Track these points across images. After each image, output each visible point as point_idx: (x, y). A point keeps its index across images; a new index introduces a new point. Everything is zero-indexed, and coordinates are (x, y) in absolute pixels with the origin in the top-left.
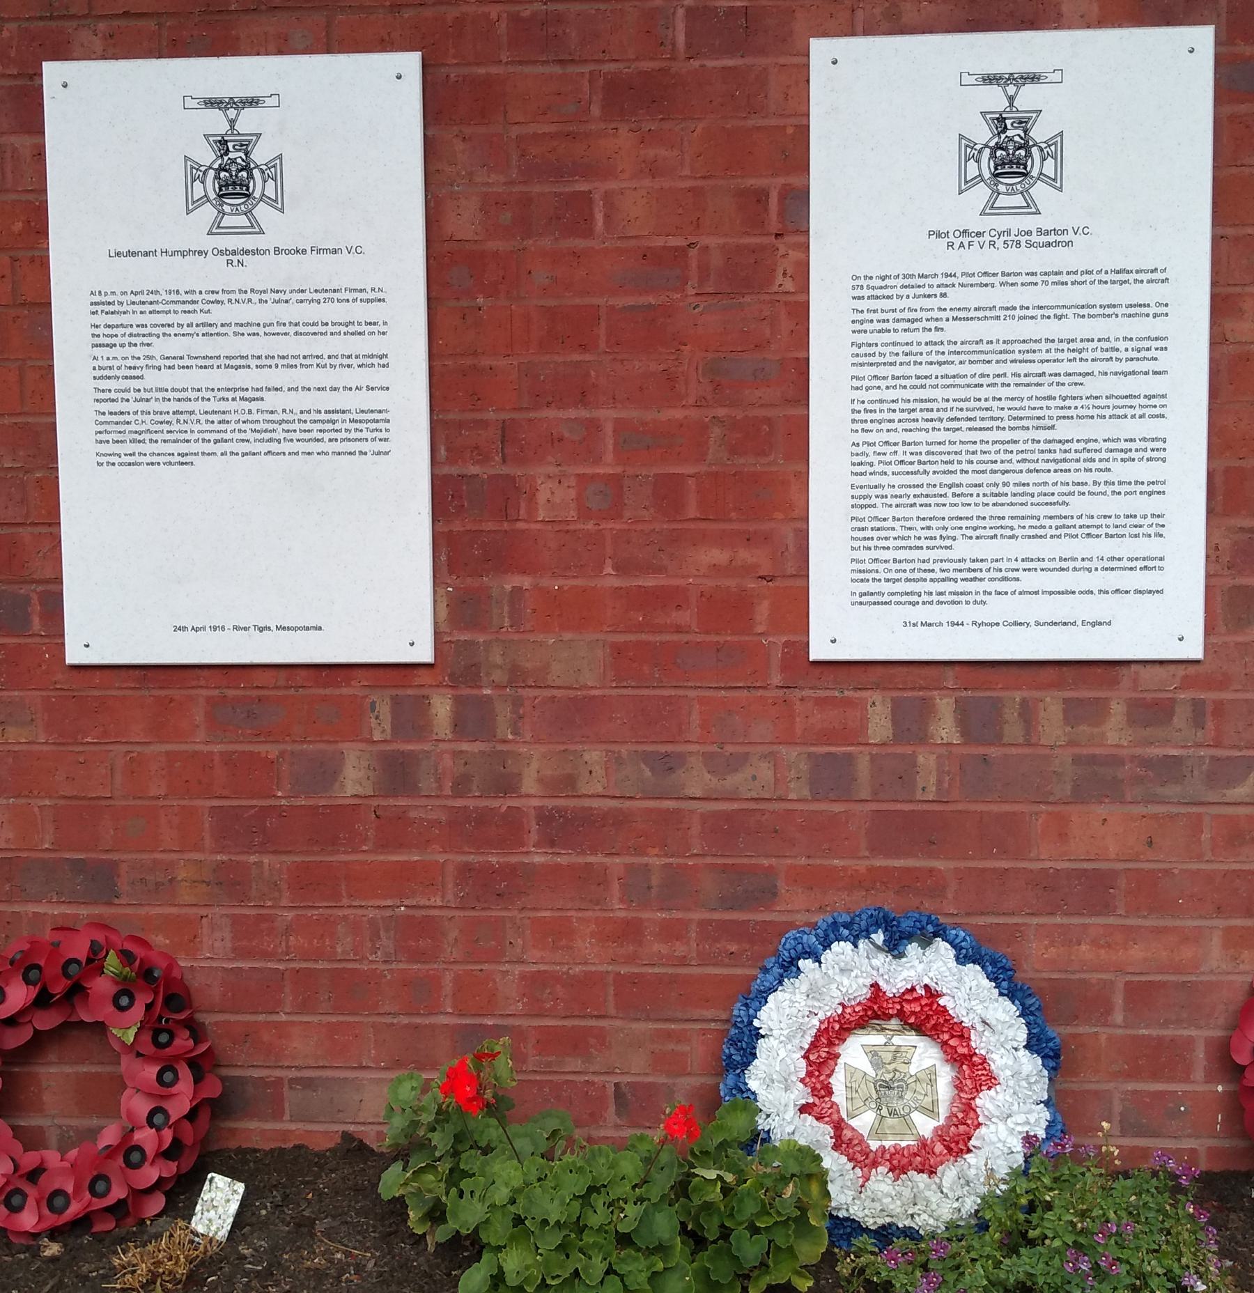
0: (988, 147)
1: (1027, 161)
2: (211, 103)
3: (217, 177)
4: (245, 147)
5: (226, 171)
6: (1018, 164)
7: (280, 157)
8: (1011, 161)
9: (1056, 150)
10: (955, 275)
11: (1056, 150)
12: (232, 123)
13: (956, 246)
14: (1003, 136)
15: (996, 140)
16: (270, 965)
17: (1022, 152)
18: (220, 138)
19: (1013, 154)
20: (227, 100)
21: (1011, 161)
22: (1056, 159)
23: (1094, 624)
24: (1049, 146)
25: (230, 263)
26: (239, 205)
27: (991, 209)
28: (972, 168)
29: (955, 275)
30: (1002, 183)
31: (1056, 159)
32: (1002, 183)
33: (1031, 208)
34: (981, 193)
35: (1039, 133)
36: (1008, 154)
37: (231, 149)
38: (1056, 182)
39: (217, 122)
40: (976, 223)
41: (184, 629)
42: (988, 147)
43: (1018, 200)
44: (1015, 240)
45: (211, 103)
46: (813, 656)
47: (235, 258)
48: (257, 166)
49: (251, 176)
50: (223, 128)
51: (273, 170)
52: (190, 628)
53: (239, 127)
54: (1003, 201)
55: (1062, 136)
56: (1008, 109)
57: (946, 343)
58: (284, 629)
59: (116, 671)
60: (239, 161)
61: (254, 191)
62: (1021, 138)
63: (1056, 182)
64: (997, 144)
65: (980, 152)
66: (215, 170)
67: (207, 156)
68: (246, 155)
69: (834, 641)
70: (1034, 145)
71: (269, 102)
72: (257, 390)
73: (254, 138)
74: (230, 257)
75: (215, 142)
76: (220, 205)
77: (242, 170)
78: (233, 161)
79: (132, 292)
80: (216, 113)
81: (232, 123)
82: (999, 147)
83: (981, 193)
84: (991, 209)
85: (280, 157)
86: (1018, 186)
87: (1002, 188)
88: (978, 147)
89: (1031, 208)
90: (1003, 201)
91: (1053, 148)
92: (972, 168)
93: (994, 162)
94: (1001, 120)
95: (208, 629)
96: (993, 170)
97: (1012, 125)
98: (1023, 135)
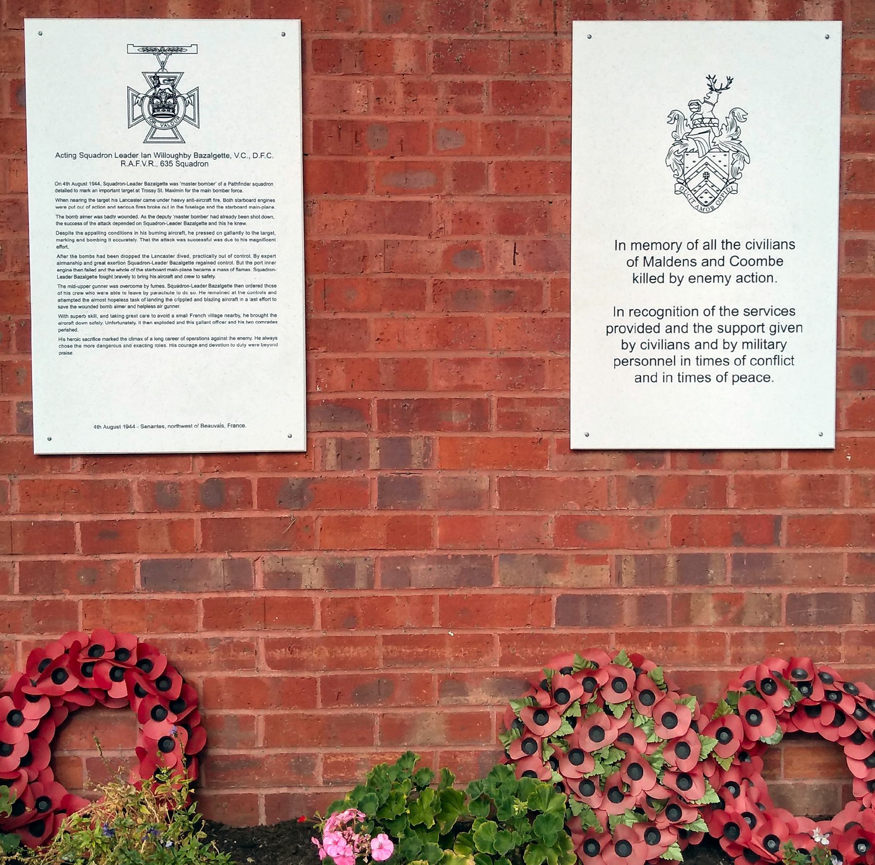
0: (147, 96)
1: (175, 106)
2: (147, 50)
3: (151, 102)
4: (172, 80)
5: (157, 98)
6: (169, 108)
7: (197, 89)
8: (164, 106)
9: (194, 99)
10: (99, 184)
11: (194, 99)
12: (163, 64)
13: (127, 163)
14: (158, 89)
15: (153, 91)
16: (346, 673)
17: (171, 101)
18: (154, 75)
19: (165, 102)
20: (159, 48)
21: (164, 106)
22: (194, 106)
23: (112, 428)
24: (189, 97)
25: (123, 163)
26: (169, 121)
27: (150, 138)
28: (138, 111)
29: (99, 184)
30: (159, 122)
31: (194, 106)
32: (159, 122)
33: (178, 139)
34: (144, 128)
35: (183, 88)
36: (162, 102)
37: (161, 82)
38: (194, 121)
39: (151, 63)
40: (142, 149)
41: (99, 427)
42: (147, 96)
43: (169, 133)
44: (167, 160)
45: (147, 50)
46: (37, 451)
47: (127, 160)
48: (180, 95)
49: (176, 103)
50: (156, 67)
51: (192, 98)
52: (103, 427)
53: (169, 67)
54: (159, 133)
55: (198, 90)
56: (161, 71)
57: (75, 233)
58: (206, 426)
59: (278, 457)
60: (167, 91)
61: (178, 111)
62: (170, 91)
63: (194, 121)
64: (154, 94)
65: (142, 99)
66: (150, 97)
67: (144, 87)
68: (173, 87)
69: (587, 435)
70: (178, 96)
71: (190, 50)
72: (101, 257)
73: (179, 75)
74: (123, 159)
75: (151, 77)
76: (153, 122)
77: (169, 98)
78: (163, 91)
79: (73, 184)
80: (151, 57)
81: (163, 64)
82: (155, 96)
83: (144, 128)
84: (150, 138)
85: (197, 89)
86: (169, 124)
87: (158, 125)
88: (141, 96)
89: (178, 139)
90: (159, 133)
91: (192, 98)
92: (138, 111)
93: (153, 106)
94: (156, 78)
95: (122, 427)
96: (151, 112)
97: (164, 81)
98: (171, 89)
